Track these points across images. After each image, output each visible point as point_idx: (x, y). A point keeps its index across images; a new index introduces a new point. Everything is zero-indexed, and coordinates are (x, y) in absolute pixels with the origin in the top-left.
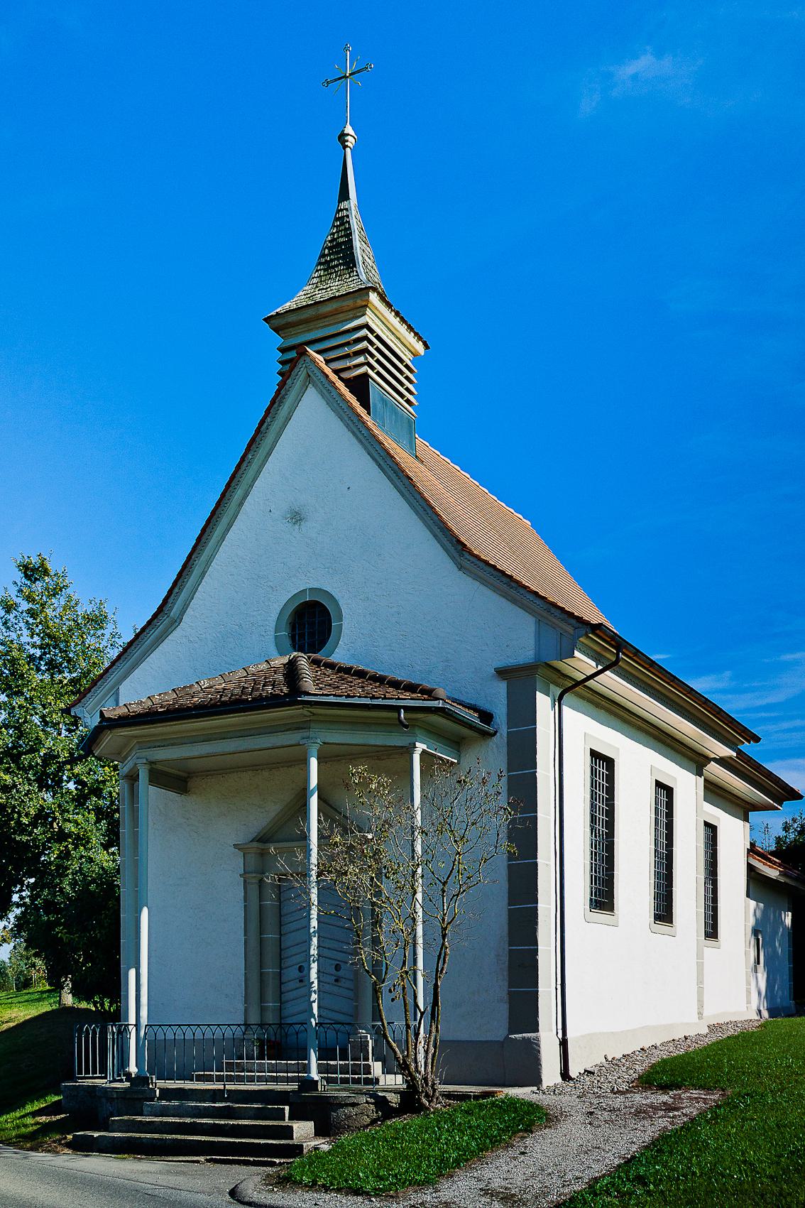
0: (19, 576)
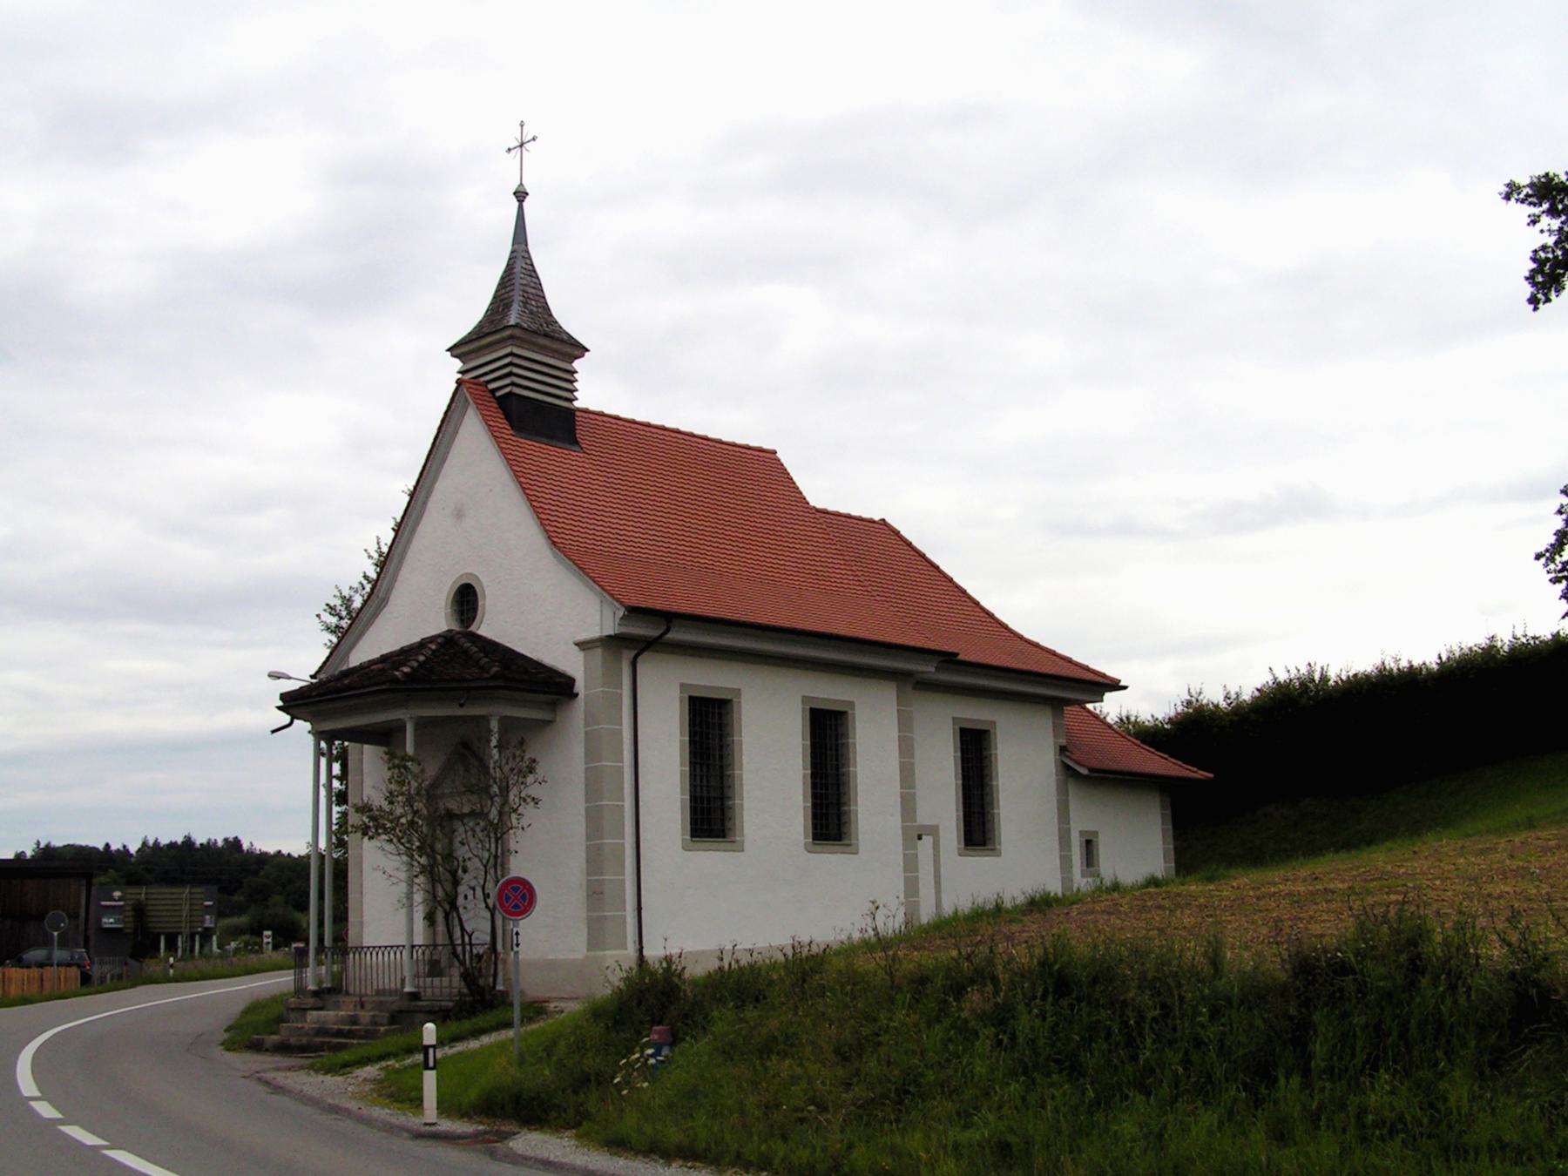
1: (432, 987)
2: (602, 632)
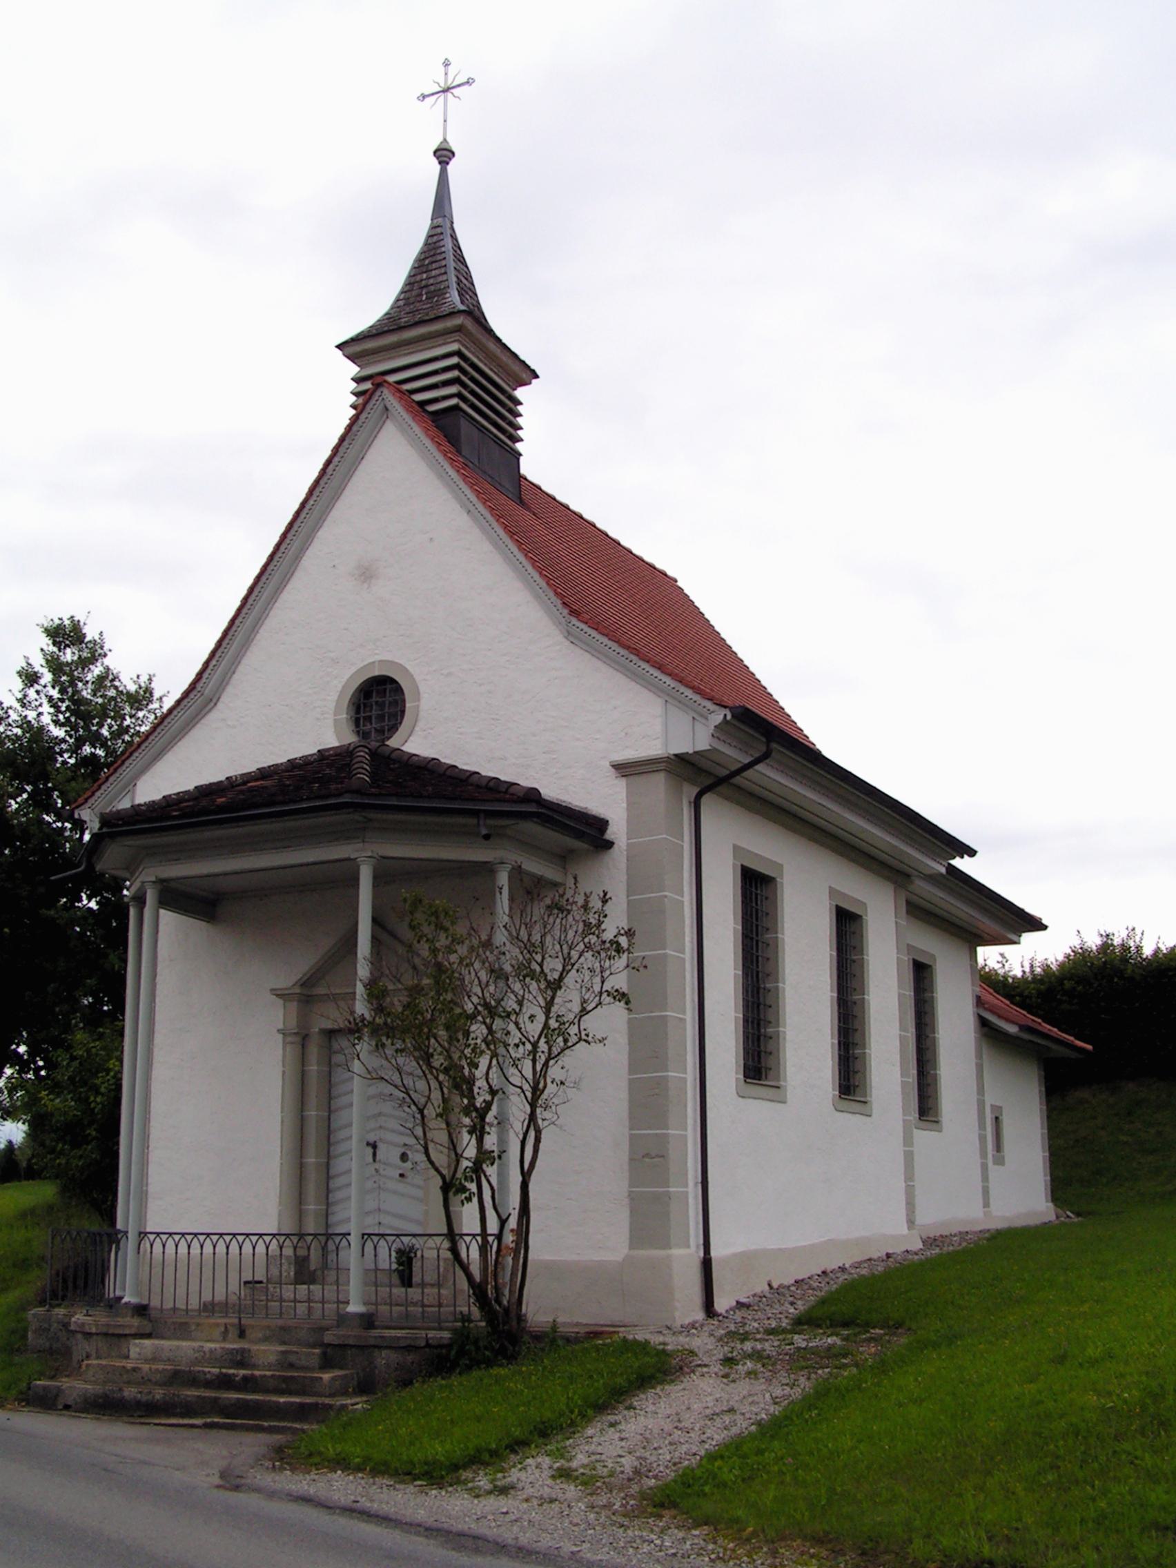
0: (46, 643)
1: (309, 1301)
2: (666, 745)
